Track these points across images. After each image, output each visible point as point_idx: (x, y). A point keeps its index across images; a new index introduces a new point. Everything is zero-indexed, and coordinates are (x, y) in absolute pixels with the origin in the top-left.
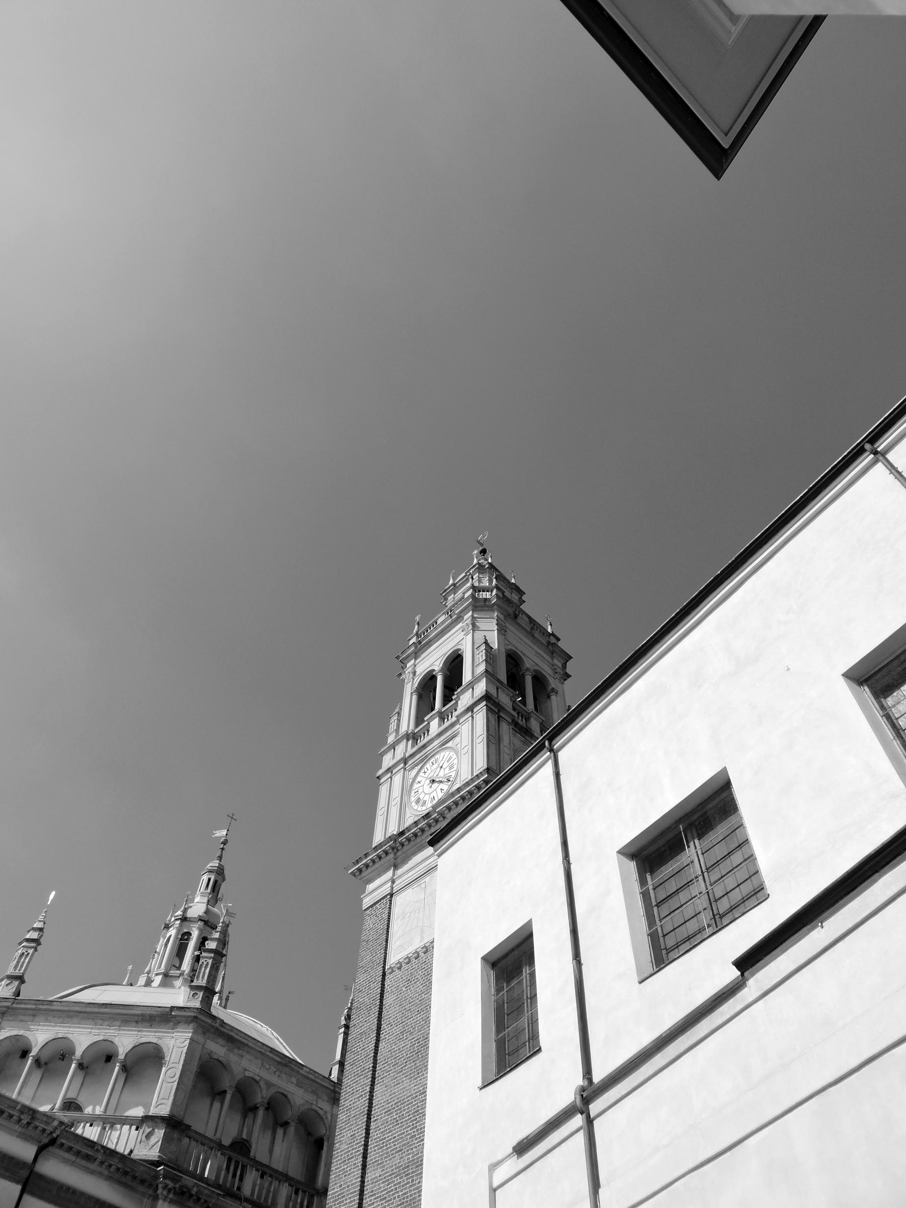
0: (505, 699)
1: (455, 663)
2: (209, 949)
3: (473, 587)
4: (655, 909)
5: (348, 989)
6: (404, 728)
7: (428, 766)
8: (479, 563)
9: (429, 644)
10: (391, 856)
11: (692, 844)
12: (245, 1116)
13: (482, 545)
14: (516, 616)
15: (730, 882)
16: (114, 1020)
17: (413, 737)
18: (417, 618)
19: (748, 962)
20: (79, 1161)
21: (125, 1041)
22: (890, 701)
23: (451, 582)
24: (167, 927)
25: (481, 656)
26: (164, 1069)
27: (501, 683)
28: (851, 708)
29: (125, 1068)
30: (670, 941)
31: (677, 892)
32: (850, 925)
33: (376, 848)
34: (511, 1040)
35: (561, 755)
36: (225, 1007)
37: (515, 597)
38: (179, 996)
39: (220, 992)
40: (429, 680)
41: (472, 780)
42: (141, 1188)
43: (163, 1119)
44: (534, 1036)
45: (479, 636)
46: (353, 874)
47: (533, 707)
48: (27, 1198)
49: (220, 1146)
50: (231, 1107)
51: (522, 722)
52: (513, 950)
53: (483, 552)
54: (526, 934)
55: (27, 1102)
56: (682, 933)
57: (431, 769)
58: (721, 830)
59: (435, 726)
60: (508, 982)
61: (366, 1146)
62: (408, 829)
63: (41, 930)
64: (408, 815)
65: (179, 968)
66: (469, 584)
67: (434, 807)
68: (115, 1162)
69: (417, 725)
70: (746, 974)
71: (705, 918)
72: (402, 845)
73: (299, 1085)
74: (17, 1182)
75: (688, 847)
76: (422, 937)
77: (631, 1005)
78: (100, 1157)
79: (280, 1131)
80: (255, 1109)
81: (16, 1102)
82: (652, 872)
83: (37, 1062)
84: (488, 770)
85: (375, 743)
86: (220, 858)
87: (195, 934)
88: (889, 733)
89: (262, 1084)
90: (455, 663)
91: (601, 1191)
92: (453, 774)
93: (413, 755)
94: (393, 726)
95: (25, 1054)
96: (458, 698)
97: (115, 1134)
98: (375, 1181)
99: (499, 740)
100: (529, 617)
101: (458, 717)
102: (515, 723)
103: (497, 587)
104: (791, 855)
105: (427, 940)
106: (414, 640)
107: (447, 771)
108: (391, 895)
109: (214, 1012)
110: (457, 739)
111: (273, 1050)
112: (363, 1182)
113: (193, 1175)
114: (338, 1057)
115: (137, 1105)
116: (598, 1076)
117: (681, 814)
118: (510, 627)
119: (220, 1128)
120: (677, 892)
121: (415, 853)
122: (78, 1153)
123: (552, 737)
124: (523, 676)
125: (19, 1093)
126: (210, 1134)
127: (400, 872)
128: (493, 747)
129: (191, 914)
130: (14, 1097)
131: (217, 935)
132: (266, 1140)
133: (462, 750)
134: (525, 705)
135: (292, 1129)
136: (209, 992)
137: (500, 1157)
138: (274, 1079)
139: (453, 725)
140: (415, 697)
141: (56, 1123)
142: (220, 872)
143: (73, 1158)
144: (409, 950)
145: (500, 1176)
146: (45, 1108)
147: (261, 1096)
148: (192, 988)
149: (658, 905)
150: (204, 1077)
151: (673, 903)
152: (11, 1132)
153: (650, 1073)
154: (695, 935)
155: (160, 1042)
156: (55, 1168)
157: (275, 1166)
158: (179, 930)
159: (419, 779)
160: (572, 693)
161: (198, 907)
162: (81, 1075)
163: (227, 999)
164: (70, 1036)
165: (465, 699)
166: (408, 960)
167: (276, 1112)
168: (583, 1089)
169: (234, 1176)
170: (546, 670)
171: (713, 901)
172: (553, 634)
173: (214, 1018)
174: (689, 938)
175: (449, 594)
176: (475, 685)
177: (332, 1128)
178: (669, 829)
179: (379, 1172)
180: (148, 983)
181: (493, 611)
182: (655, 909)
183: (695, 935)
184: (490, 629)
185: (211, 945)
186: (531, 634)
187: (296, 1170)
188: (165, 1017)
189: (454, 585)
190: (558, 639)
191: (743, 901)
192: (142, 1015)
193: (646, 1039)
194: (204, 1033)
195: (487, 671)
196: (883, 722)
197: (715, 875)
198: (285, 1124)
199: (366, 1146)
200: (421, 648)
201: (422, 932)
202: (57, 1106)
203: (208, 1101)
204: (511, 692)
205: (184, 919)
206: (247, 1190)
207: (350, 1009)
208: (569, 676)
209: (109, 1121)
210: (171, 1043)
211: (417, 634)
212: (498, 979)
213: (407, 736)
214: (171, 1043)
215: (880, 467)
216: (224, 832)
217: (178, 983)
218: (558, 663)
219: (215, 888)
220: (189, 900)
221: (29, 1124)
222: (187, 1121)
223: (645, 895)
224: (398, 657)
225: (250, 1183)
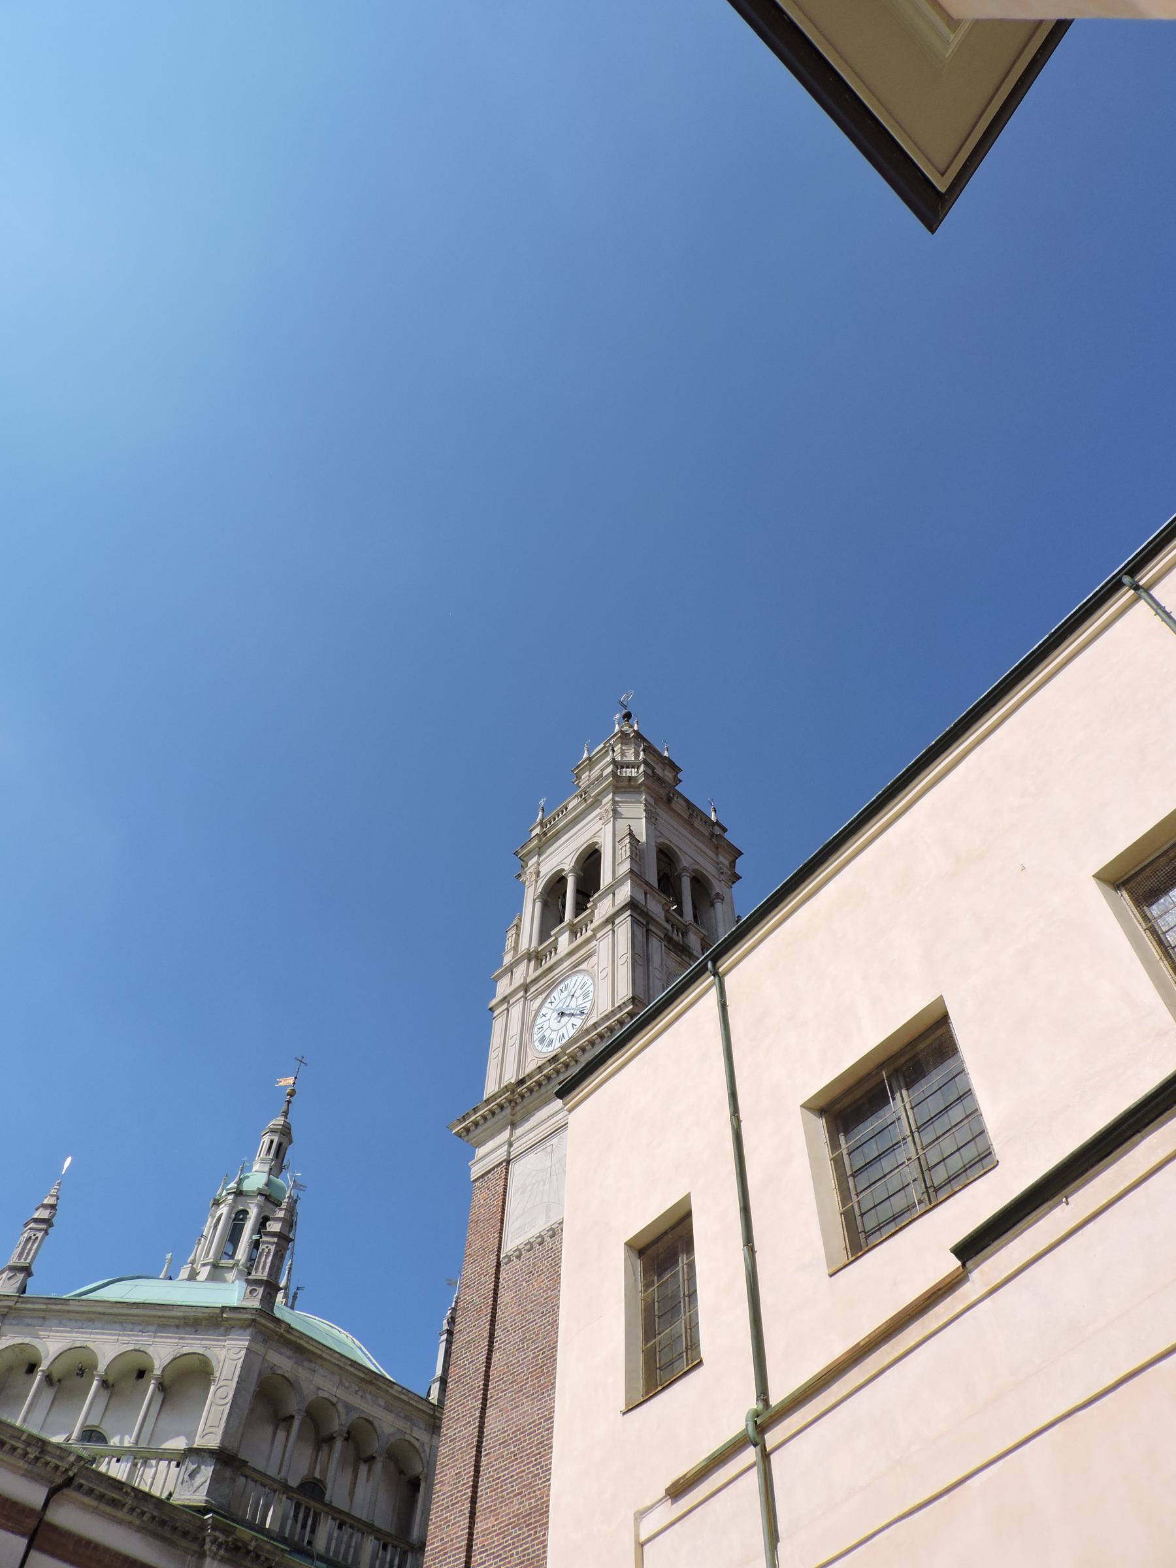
0: (655, 907)
1: (590, 860)
2: (271, 1233)
3: (614, 762)
5: (451, 1283)
6: (524, 946)
7: (555, 994)
8: (621, 731)
9: (557, 836)
10: (508, 1111)
11: (898, 1095)
12: (318, 1449)
13: (625, 707)
14: (670, 800)
15: (948, 1145)
16: (149, 1324)
17: (536, 957)
18: (542, 802)
19: (972, 1249)
21: (162, 1351)
22: (1155, 910)
23: (585, 755)
24: (217, 1203)
25: (625, 851)
26: (212, 1388)
27: (651, 886)
28: (1105, 919)
29: (162, 1387)
30: (870, 1222)
31: (878, 1158)
32: (1104, 1201)
33: (488, 1101)
34: (663, 1350)
35: (728, 980)
36: (292, 1308)
37: (668, 775)
38: (232, 1293)
39: (286, 1288)
40: (557, 883)
41: (613, 1013)
42: (183, 1543)
43: (211, 1452)
44: (693, 1345)
45: (622, 825)
46: (458, 1134)
47: (691, 918)
48: (35, 1555)
49: (286, 1488)
50: (300, 1436)
51: (677, 938)
52: (666, 1233)
53: (628, 716)
55: (35, 1431)
56: (885, 1211)
57: (559, 998)
58: (936, 1077)
60: (660, 1276)
61: (475, 1487)
62: (530, 1076)
63: (53, 1207)
64: (529, 1058)
65: (232, 1257)
67: (564, 1048)
68: (148, 1508)
69: (541, 941)
70: (969, 1264)
71: (915, 1192)
72: (522, 1097)
74: (23, 1535)
75: (893, 1100)
76: (548, 1217)
77: (820, 1304)
78: (129, 1502)
79: (363, 1468)
80: (330, 1439)
83: (48, 1379)
84: (633, 999)
85: (487, 964)
86: (286, 1114)
87: (253, 1212)
89: (340, 1407)
90: (590, 860)
92: (588, 1005)
93: (535, 981)
94: (510, 943)
95: (32, 1368)
96: (595, 905)
97: (149, 1472)
98: (486, 1533)
99: (648, 960)
100: (687, 801)
101: (595, 931)
102: (669, 939)
103: (645, 762)
104: (1027, 1110)
105: (554, 1220)
106: (537, 831)
107: (580, 1000)
108: (508, 1162)
109: (277, 1313)
110: (594, 959)
111: (354, 1363)
112: (471, 1534)
113: (250, 1525)
114: (439, 1372)
116: (775, 1399)
118: (662, 813)
120: (878, 1158)
121: (538, 1108)
122: (101, 1497)
123: (716, 957)
124: (679, 878)
125: (25, 1420)
126: (272, 1472)
127: (519, 1131)
128: (640, 969)
130: (18, 1424)
131: (281, 1214)
133: (599, 974)
134: (681, 915)
135: (378, 1466)
136: (271, 1287)
137: (649, 1503)
138: (355, 1401)
139: (587, 941)
140: (538, 905)
141: (72, 1458)
142: (285, 1132)
143: (95, 1503)
144: (531, 1233)
145: (648, 1527)
146: (58, 1439)
147: (338, 1423)
149: (854, 1175)
150: (264, 1398)
151: (874, 1173)
152: (14, 1469)
155: (207, 1353)
156: (71, 1516)
157: (357, 1513)
158: (232, 1207)
159: (543, 1011)
161: (256, 1179)
162: (105, 1394)
163: (295, 1297)
165: (603, 908)
166: (530, 1246)
167: (358, 1443)
168: (757, 1414)
169: (304, 1526)
170: (709, 870)
171: (926, 1170)
172: (717, 823)
173: (278, 1321)
174: (894, 1218)
175: (583, 771)
176: (616, 889)
178: (869, 1075)
179: (492, 1521)
180: (193, 1276)
181: (640, 793)
182: (851, 1180)
184: (636, 817)
185: (274, 1227)
186: (689, 823)
187: (384, 1518)
188: (215, 1321)
189: (589, 759)
190: (725, 830)
191: (966, 1169)
193: (839, 1349)
194: (265, 1341)
195: (632, 871)
196: (1147, 938)
198: (370, 1460)
199: (475, 1487)
200: (546, 841)
202: (74, 1436)
203: (269, 1430)
204: (663, 898)
205: (239, 1193)
206: (320, 1545)
207: (454, 1310)
209: (141, 1456)
211: (541, 823)
212: (646, 1272)
213: (529, 956)
215: (1142, 607)
216: (291, 1081)
217: (231, 1276)
218: (724, 860)
219: (280, 1152)
221: (37, 1459)
222: (243, 1456)
223: (838, 1162)
224: (516, 853)
225: (325, 1535)
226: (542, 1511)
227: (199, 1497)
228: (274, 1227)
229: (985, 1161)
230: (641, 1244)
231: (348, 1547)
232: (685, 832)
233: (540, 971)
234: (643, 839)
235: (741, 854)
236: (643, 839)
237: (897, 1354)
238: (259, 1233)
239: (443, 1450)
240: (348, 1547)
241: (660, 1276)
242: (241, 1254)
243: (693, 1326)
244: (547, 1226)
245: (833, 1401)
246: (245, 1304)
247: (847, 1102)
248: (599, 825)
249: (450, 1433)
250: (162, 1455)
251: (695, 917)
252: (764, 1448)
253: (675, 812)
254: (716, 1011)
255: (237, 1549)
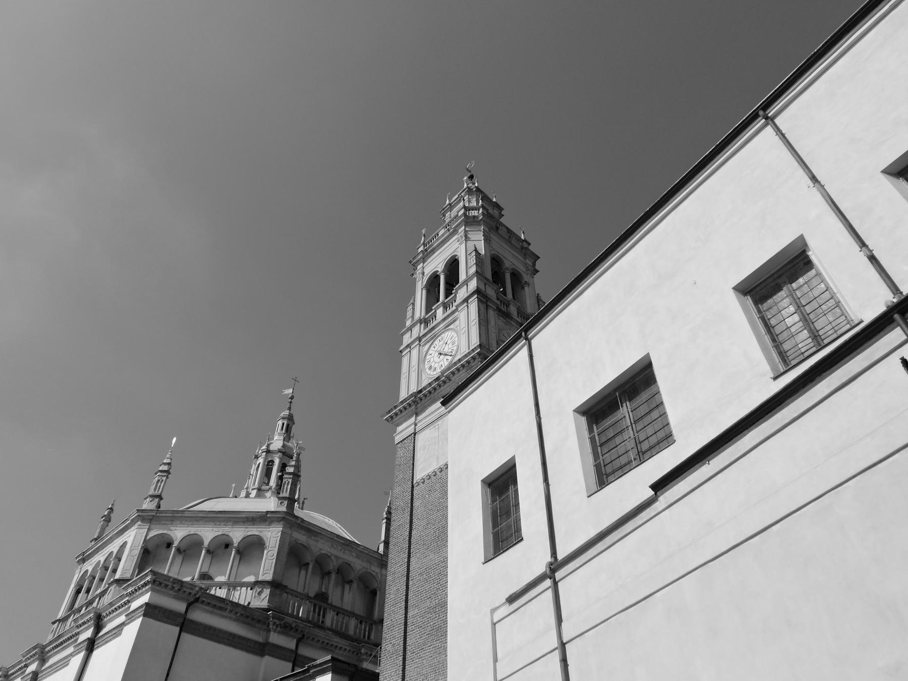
0: (491, 292)
1: (453, 265)
2: (286, 471)
3: (464, 207)
7: (436, 342)
8: (468, 187)
9: (433, 251)
10: (413, 407)
11: (624, 405)
12: (323, 578)
13: (470, 171)
14: (497, 229)
15: (650, 430)
17: (425, 322)
18: (424, 231)
19: (659, 486)
20: (215, 611)
21: (237, 534)
22: (765, 306)
23: (448, 202)
24: (257, 457)
25: (473, 260)
26: (265, 552)
27: (488, 280)
28: (737, 315)
29: (238, 552)
30: (609, 469)
31: (614, 437)
32: (727, 463)
33: (402, 402)
34: (503, 532)
35: (534, 342)
36: (302, 509)
37: (495, 213)
38: (270, 504)
40: (434, 279)
41: (469, 353)
42: (258, 625)
43: (268, 582)
44: (518, 530)
45: (471, 245)
46: (387, 420)
47: (514, 303)
48: (184, 635)
49: (308, 597)
50: (313, 573)
51: (504, 309)
52: (502, 475)
53: (471, 177)
55: (176, 577)
56: (617, 464)
57: (438, 344)
58: (644, 396)
59: (440, 312)
61: (407, 595)
62: (425, 388)
63: (169, 464)
64: (424, 377)
65: (268, 484)
66: (461, 204)
67: (443, 372)
69: (427, 312)
71: (632, 455)
72: (421, 399)
73: (358, 557)
74: (177, 625)
75: (623, 410)
77: (583, 511)
79: (347, 587)
80: (329, 573)
81: (167, 578)
82: (597, 424)
83: (179, 550)
84: (480, 346)
85: (399, 329)
86: (290, 409)
87: (277, 461)
89: (333, 557)
90: (453, 265)
92: (455, 348)
94: (409, 314)
95: (169, 545)
96: (457, 292)
97: (237, 593)
98: (414, 616)
100: (508, 229)
101: (457, 307)
102: (499, 310)
103: (483, 206)
104: (692, 411)
105: (441, 463)
106: (421, 249)
107: (450, 346)
108: (415, 434)
109: (296, 513)
110: (457, 323)
111: (338, 536)
112: (406, 617)
113: (292, 616)
114: (383, 538)
115: (250, 575)
116: (560, 557)
118: (493, 237)
119: (307, 586)
120: (614, 437)
121: (430, 405)
122: (214, 606)
123: (527, 329)
124: (504, 273)
125: (169, 571)
126: (300, 590)
127: (420, 418)
128: (483, 328)
129: (272, 448)
130: (166, 573)
131: (293, 463)
132: (338, 591)
133: (460, 333)
134: (505, 295)
135: (355, 585)
136: (291, 501)
137: (497, 605)
138: (341, 555)
139: (453, 312)
140: (424, 292)
141: (197, 589)
142: (290, 418)
143: (211, 609)
144: (430, 470)
145: (497, 616)
147: (332, 565)
148: (279, 498)
149: (601, 446)
150: (292, 555)
151: (611, 445)
152: (169, 595)
154: (625, 465)
155: (261, 534)
156: (200, 616)
157: (345, 607)
158: (265, 459)
159: (430, 352)
161: (277, 443)
162: (209, 557)
163: (303, 503)
165: (461, 293)
166: (429, 477)
167: (343, 574)
168: (551, 564)
169: (319, 615)
170: (521, 268)
171: (638, 443)
172: (525, 240)
173: (297, 517)
174: (621, 467)
175: (446, 212)
176: (468, 284)
178: (609, 394)
179: (416, 611)
180: (248, 496)
181: (480, 225)
183: (625, 465)
184: (478, 239)
185: (290, 470)
187: (359, 609)
188: (264, 518)
189: (450, 204)
190: (529, 244)
191: (658, 443)
192: (247, 518)
193: (592, 533)
194: (291, 528)
195: (477, 272)
196: (759, 323)
197: (640, 426)
198: (350, 582)
199: (407, 595)
200: (427, 255)
201: (438, 459)
202: (196, 577)
203: (297, 570)
204: (495, 287)
205: (268, 451)
206: (328, 623)
207: (389, 507)
208: (537, 271)
209: (232, 585)
211: (424, 244)
212: (493, 495)
213: (420, 321)
214: (269, 534)
215: (769, 129)
216: (291, 391)
217: (268, 494)
218: (529, 262)
220: (270, 438)
221: (179, 590)
222: (284, 583)
223: (592, 440)
225: (330, 619)
226: (444, 605)
227: (264, 604)
229: (669, 439)
230: (490, 481)
231: (342, 623)
232: (506, 246)
233: (427, 330)
234: (483, 252)
236: (483, 252)
237: (621, 536)
239: (389, 578)
240: (342, 623)
242: (273, 482)
243: (518, 521)
244: (438, 466)
245: (589, 557)
249: (392, 570)
250: (242, 585)
251: (513, 295)
252: (555, 579)
254: (527, 359)
255: (286, 627)
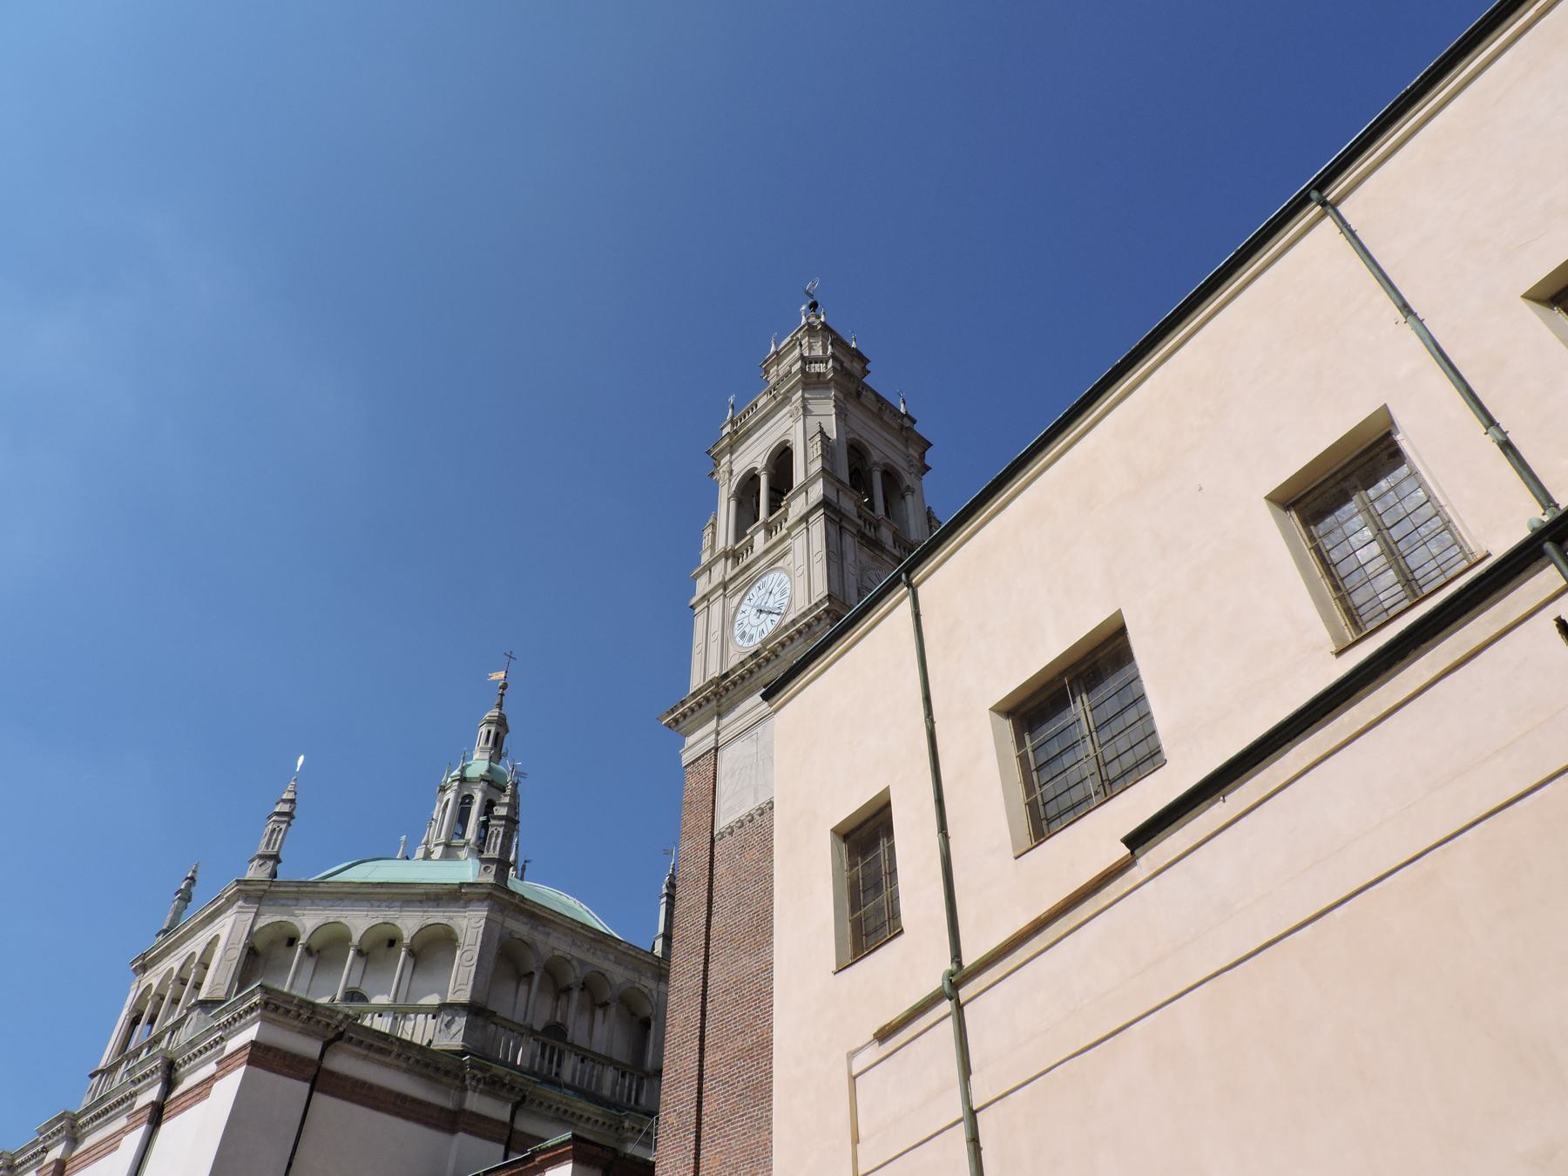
0: (847, 504)
1: (782, 458)
2: (495, 815)
3: (802, 357)
4: (1035, 775)
5: (668, 853)
6: (721, 545)
7: (753, 591)
9: (748, 434)
11: (1078, 699)
12: (557, 999)
13: (811, 296)
14: (859, 395)
15: (1122, 743)
16: (393, 900)
17: (734, 555)
18: (731, 400)
19: (1138, 840)
20: (372, 1054)
21: (409, 923)
23: (773, 349)
24: (443, 789)
25: (816, 449)
26: (458, 953)
27: (842, 483)
28: (1273, 543)
29: (412, 953)
30: (1052, 810)
32: (1256, 800)
33: (694, 695)
34: (868, 919)
35: (922, 591)
37: (856, 367)
38: (466, 870)
39: (516, 861)
40: (750, 482)
41: (810, 610)
42: (445, 1079)
43: (462, 1006)
44: (895, 915)
45: (813, 422)
46: (668, 725)
47: (886, 524)
48: (318, 1098)
49: (532, 1032)
50: (541, 989)
51: (870, 533)
52: (868, 820)
53: (814, 306)
54: (882, 802)
55: (303, 995)
56: (1066, 801)
57: (756, 595)
58: (1113, 683)
59: (759, 538)
60: (863, 858)
61: (703, 1028)
62: (733, 670)
63: (292, 801)
65: (462, 836)
66: (797, 352)
67: (765, 643)
68: (413, 1053)
69: (737, 541)
70: (1137, 852)
71: (1091, 785)
72: (727, 689)
73: (617, 962)
74: (498, 1141)
75: (1076, 708)
76: (756, 799)
77: (1007, 882)
78: (396, 1049)
79: (599, 1013)
81: (289, 998)
82: (1031, 732)
83: (308, 950)
84: (829, 597)
85: (687, 566)
86: (500, 706)
87: (478, 797)
88: (1317, 570)
89: (575, 963)
90: (782, 458)
91: (974, 1079)
92: (786, 601)
93: (733, 579)
94: (707, 542)
95: (292, 941)
96: (789, 504)
97: (409, 1025)
98: (715, 1064)
99: (842, 556)
100: (876, 395)
101: (790, 529)
102: (861, 535)
103: (833, 356)
104: (1196, 710)
105: (762, 800)
106: (728, 429)
107: (778, 597)
108: (716, 749)
109: (511, 886)
110: (789, 557)
111: (584, 926)
112: (701, 1066)
113: (504, 1063)
114: (661, 929)
115: (431, 993)
116: (968, 961)
117: (1064, 666)
119: (530, 1012)
121: (742, 700)
122: (370, 1047)
123: (910, 569)
124: (870, 472)
125: (292, 985)
126: (518, 1018)
127: (725, 721)
129: (469, 773)
130: (286, 989)
131: (506, 800)
132: (584, 1022)
133: (794, 574)
134: (872, 509)
135: (612, 1011)
136: (503, 865)
138: (588, 958)
140: (733, 504)
141: (340, 1017)
142: (501, 722)
143: (365, 1052)
144: (742, 812)
145: (859, 1064)
146: (324, 1000)
147: (573, 976)
148: (482, 861)
149: (1037, 770)
150: (505, 958)
151: (1055, 768)
152: (292, 1029)
153: (1028, 956)
155: (450, 923)
156: (344, 1063)
157: (596, 1049)
158: (458, 793)
159: (743, 608)
160: (938, 492)
161: (478, 765)
162: (361, 962)
163: (524, 868)
164: (343, 920)
165: (797, 507)
166: (741, 824)
167: (593, 992)
168: (952, 974)
169: (551, 1061)
170: (900, 463)
171: (1102, 764)
172: (907, 415)
173: (513, 894)
174: (1073, 807)
175: (771, 365)
176: (808, 491)
177: (662, 1006)
178: (1052, 682)
180: (427, 856)
181: (829, 389)
182: (1035, 775)
184: (826, 413)
185: (501, 811)
186: (878, 416)
187: (621, 1052)
188: (456, 895)
189: (777, 353)
190: (914, 422)
191: (1137, 765)
192: (426, 894)
193: (1023, 921)
194: (502, 911)
195: (823, 469)
197: (1105, 735)
198: (605, 1005)
199: (703, 1028)
201: (756, 792)
202: (338, 997)
203: (513, 985)
204: (855, 495)
205: (463, 780)
206: (566, 1075)
207: (672, 876)
208: (927, 468)
209: (400, 1011)
210: (464, 923)
212: (851, 854)
214: (464, 923)
215: (1328, 223)
216: (502, 675)
217: (463, 853)
218: (913, 452)
219: (498, 742)
220: (467, 757)
221: (309, 1018)
222: (490, 1007)
223: (1023, 759)
224: (708, 452)
225: (569, 1069)
228: (502, 811)
229: (1156, 758)
231: (591, 1076)
233: (737, 569)
234: (833, 435)
235: (930, 445)
236: (833, 435)
238: (486, 814)
240: (591, 1076)
241: (863, 858)
242: (471, 833)
244: (756, 805)
246: (481, 880)
247: (1034, 703)
248: (790, 422)
250: (419, 1010)
251: (886, 509)
253: (865, 407)
254: (910, 620)
255: (494, 1083)
